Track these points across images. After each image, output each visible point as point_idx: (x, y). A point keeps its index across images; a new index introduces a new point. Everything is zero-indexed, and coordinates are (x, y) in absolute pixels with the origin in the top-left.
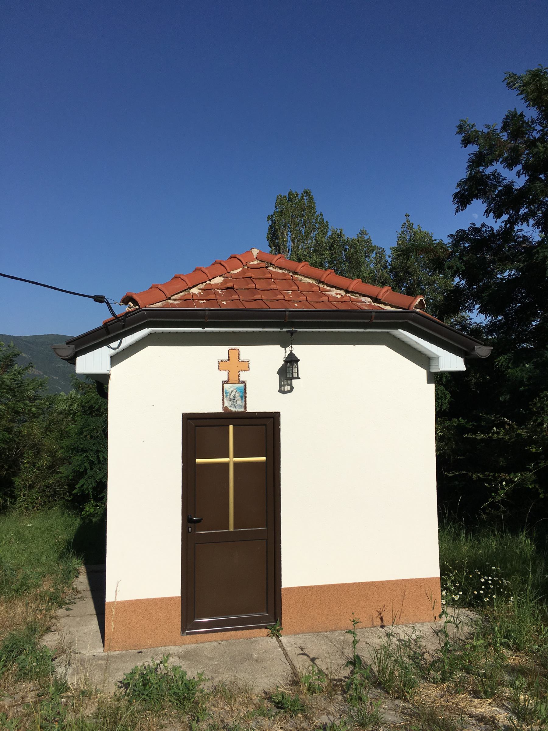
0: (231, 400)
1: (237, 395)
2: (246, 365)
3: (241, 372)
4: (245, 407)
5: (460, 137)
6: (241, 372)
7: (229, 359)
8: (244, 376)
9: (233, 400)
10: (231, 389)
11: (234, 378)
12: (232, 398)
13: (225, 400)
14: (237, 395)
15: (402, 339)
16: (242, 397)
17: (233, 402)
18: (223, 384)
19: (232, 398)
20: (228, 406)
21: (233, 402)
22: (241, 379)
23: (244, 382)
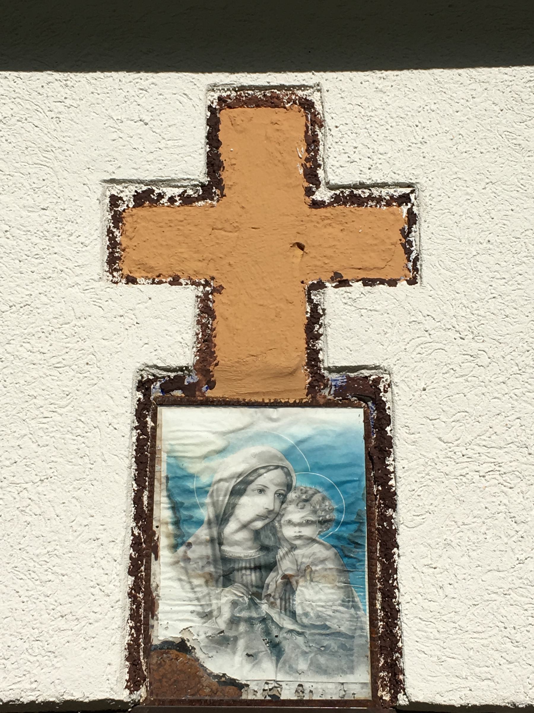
0: (224, 572)
1: (295, 521)
2: (383, 229)
3: (332, 298)
4: (385, 647)
5: (403, 285)
6: (332, 298)
7: (213, 185)
8: (357, 329)
9: (254, 575)
10: (235, 464)
11: (261, 338)
12: (239, 546)
13: (165, 573)
14: (295, 521)
15: (133, 472)
16: (344, 548)
17: (257, 593)
18: (145, 410)
19: (239, 546)
20: (198, 633)
21: (257, 593)
22: (338, 351)
23: (364, 391)
